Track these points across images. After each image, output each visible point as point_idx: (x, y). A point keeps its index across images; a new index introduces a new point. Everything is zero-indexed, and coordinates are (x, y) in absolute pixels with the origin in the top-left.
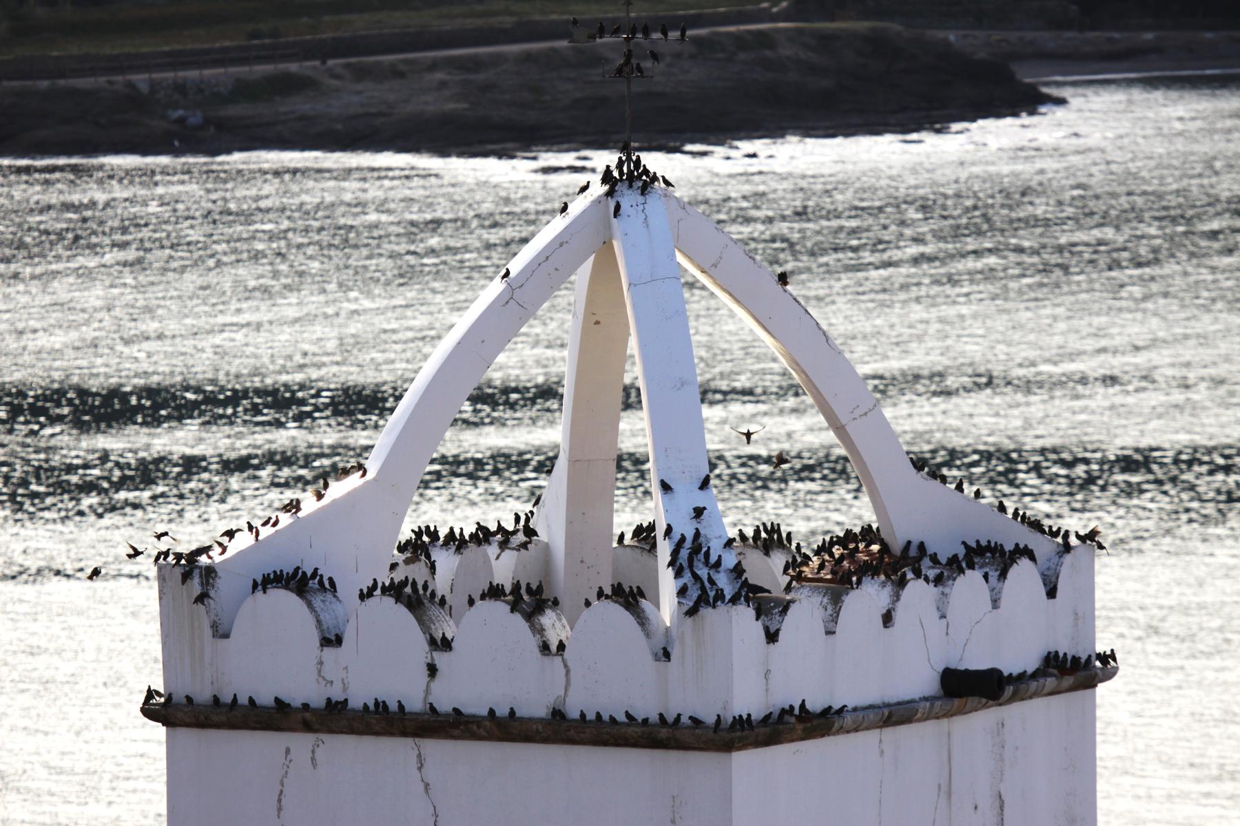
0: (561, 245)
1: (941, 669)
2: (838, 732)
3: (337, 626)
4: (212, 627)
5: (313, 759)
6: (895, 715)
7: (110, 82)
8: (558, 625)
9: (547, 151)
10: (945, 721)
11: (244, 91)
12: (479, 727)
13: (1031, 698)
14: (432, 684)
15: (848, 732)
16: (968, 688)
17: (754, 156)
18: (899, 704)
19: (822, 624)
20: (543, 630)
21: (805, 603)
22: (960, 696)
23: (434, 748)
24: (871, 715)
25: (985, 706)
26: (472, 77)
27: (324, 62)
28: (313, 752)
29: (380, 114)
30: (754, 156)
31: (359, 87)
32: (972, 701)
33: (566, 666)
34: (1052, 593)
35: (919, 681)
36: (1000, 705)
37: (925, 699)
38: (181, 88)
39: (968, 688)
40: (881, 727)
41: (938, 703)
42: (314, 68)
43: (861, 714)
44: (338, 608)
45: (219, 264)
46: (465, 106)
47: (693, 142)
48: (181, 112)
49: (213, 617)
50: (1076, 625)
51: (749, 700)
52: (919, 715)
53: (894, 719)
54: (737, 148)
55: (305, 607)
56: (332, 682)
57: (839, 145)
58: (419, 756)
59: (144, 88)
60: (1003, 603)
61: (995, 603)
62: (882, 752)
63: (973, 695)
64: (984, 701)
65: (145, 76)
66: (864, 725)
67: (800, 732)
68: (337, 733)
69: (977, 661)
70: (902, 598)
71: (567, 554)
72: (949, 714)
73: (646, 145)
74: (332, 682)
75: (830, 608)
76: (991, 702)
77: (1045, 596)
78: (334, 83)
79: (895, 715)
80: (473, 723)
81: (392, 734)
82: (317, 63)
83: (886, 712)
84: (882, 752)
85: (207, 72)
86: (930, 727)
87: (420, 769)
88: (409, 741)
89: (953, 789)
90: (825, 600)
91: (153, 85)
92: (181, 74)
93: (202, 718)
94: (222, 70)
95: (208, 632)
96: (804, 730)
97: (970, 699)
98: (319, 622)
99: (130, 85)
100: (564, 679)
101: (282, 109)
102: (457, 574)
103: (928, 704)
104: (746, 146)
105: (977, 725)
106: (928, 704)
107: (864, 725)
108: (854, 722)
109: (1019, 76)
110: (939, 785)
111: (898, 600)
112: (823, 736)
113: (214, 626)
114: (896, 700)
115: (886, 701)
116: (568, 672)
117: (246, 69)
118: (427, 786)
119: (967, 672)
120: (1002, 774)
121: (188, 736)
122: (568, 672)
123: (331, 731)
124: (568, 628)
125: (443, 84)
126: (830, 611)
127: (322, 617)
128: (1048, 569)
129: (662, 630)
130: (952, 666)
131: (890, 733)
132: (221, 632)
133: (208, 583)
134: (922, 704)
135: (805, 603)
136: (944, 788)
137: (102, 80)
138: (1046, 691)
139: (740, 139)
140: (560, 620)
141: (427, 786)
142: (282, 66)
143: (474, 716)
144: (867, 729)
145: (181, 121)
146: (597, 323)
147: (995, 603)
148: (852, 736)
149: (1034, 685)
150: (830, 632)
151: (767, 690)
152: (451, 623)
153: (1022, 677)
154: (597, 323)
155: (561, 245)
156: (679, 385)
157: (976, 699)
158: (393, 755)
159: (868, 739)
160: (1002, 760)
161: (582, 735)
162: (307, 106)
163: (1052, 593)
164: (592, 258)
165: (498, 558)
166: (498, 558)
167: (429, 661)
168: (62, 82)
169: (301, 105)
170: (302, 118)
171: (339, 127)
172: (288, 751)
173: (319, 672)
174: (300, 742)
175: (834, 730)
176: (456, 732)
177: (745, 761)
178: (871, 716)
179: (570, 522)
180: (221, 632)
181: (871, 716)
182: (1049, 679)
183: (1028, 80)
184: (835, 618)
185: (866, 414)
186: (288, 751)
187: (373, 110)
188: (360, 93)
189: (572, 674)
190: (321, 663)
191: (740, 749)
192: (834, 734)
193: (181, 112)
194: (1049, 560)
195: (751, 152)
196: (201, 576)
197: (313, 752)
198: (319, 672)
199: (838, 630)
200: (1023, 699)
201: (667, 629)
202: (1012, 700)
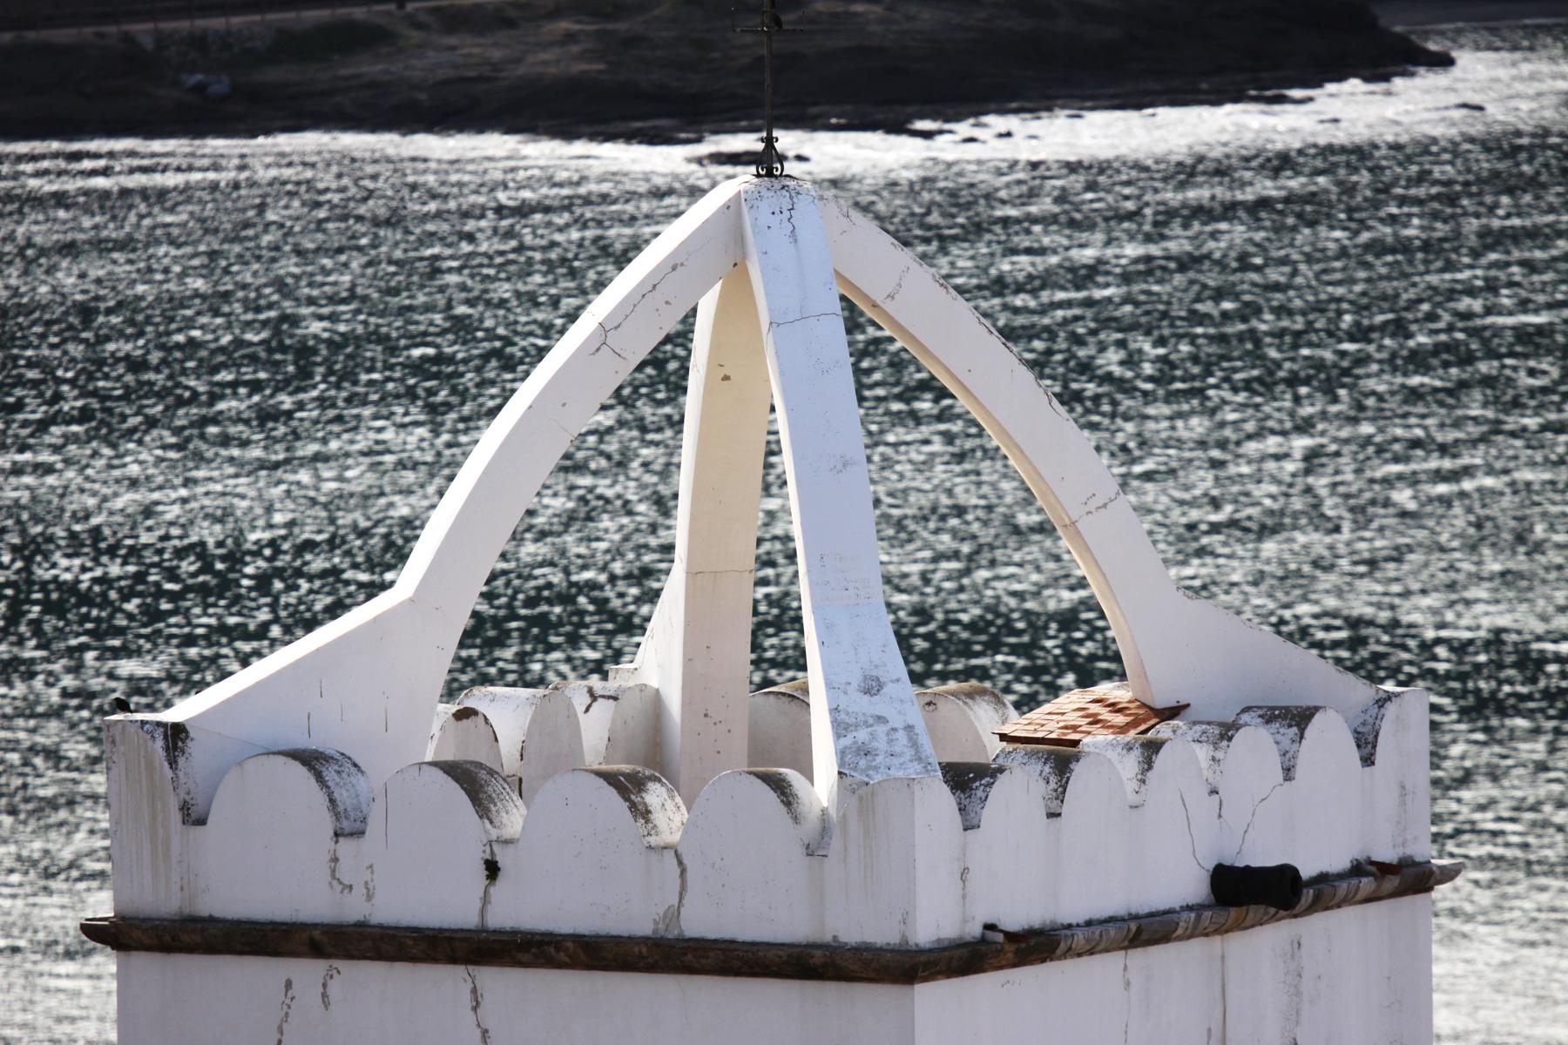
0: (674, 268)
1: (1211, 866)
2: (1064, 956)
3: (358, 808)
4: (182, 809)
5: (324, 995)
6: (1145, 930)
7: (100, 35)
8: (669, 805)
9: (1477, 48)
10: (1217, 939)
11: (290, 46)
12: (558, 949)
13: (1339, 906)
14: (492, 890)
15: (1079, 955)
16: (1252, 893)
17: (1009, 134)
18: (1151, 915)
19: (1042, 803)
20: (649, 812)
21: (1018, 771)
22: (1238, 904)
23: (497, 981)
24: (1112, 930)
25: (1274, 918)
26: (610, 26)
27: (401, 5)
28: (324, 985)
29: (480, 79)
30: (1009, 134)
31: (452, 40)
32: (1255, 911)
33: (680, 863)
34: (1368, 761)
35: (1183, 884)
36: (1296, 916)
37: (1189, 908)
38: (199, 42)
39: (1252, 893)
40: (1125, 948)
41: (1207, 914)
42: (389, 13)
43: (1097, 930)
44: (360, 783)
45: (491, 258)
46: (601, 66)
47: (922, 117)
48: (199, 77)
49: (183, 795)
50: (1403, 803)
51: (935, 920)
52: (1180, 931)
53: (1144, 937)
54: (985, 125)
55: (313, 780)
56: (351, 887)
57: (1228, 114)
58: (474, 991)
59: (148, 42)
60: (1299, 772)
61: (1288, 773)
62: (1128, 983)
63: (1256, 903)
64: (1272, 910)
65: (149, 26)
66: (1102, 946)
67: (1010, 955)
68: (359, 958)
69: (1261, 852)
70: (1156, 766)
71: (687, 702)
72: (1221, 930)
73: (856, 122)
74: (351, 887)
75: (1053, 779)
76: (1282, 913)
77: (1358, 762)
78: (416, 36)
79: (1145, 930)
80: (549, 943)
81: (435, 960)
82: (392, 7)
83: (1133, 926)
84: (1128, 983)
85: (236, 21)
86: (1195, 949)
87: (475, 1009)
88: (460, 971)
89: (1229, 1034)
90: (1047, 769)
91: (161, 40)
92: (201, 23)
93: (167, 938)
94: (257, 18)
95: (176, 817)
96: (1017, 952)
97: (1252, 907)
98: (332, 801)
99: (128, 38)
100: (678, 881)
101: (344, 72)
102: (529, 733)
103: (1193, 915)
104: (997, 122)
105: (1262, 946)
106: (1193, 915)
107: (1102, 946)
108: (1088, 941)
109: (1383, 22)
110: (1209, 1030)
111: (1150, 768)
112: (1043, 961)
113: (185, 808)
114: (1146, 911)
115: (1133, 911)
116: (683, 872)
117: (291, 15)
118: (485, 1032)
119: (1248, 869)
120: (1298, 1013)
121: (140, 959)
122: (683, 872)
123: (350, 956)
124: (683, 809)
125: (570, 37)
126: (1053, 785)
127: (336, 795)
128: (1364, 724)
129: (817, 812)
130: (1227, 862)
131: (1140, 958)
132: (194, 817)
133: (175, 747)
134: (1185, 915)
135: (1018, 771)
136: (1216, 1032)
137: (88, 31)
138: (1359, 896)
139: (986, 113)
140: (672, 798)
141: (485, 1032)
142: (342, 11)
143: (533, 934)
144: (1107, 950)
145: (200, 88)
146: (726, 378)
147: (1288, 773)
148: (1085, 959)
149: (1343, 887)
150: (1053, 815)
151: (964, 897)
152: (519, 802)
153: (1323, 878)
154: (726, 378)
155: (674, 268)
156: (839, 466)
157: (1262, 908)
158: (445, 984)
159: (1105, 970)
160: (1298, 994)
161: (704, 961)
162: (379, 67)
163: (1368, 761)
164: (718, 286)
165: (587, 710)
166: (587, 710)
167: (488, 856)
168: (31, 35)
169: (369, 67)
170: (373, 85)
171: (423, 96)
172: (289, 985)
173: (333, 871)
174: (306, 972)
175: (1058, 952)
176: (526, 957)
177: (932, 997)
178: (1112, 933)
179: (688, 660)
180: (194, 816)
181: (1112, 933)
182: (1365, 880)
183: (1398, 29)
184: (1061, 794)
185: (1105, 506)
186: (289, 985)
187: (472, 74)
188: (453, 48)
189: (690, 875)
190: (335, 860)
191: (925, 979)
192: (1059, 958)
193: (199, 77)
194: (1365, 712)
195: (1003, 130)
196: (166, 737)
197: (324, 985)
198: (333, 871)
199: (1065, 810)
200: (1327, 909)
201: (824, 811)
202: (1312, 909)
